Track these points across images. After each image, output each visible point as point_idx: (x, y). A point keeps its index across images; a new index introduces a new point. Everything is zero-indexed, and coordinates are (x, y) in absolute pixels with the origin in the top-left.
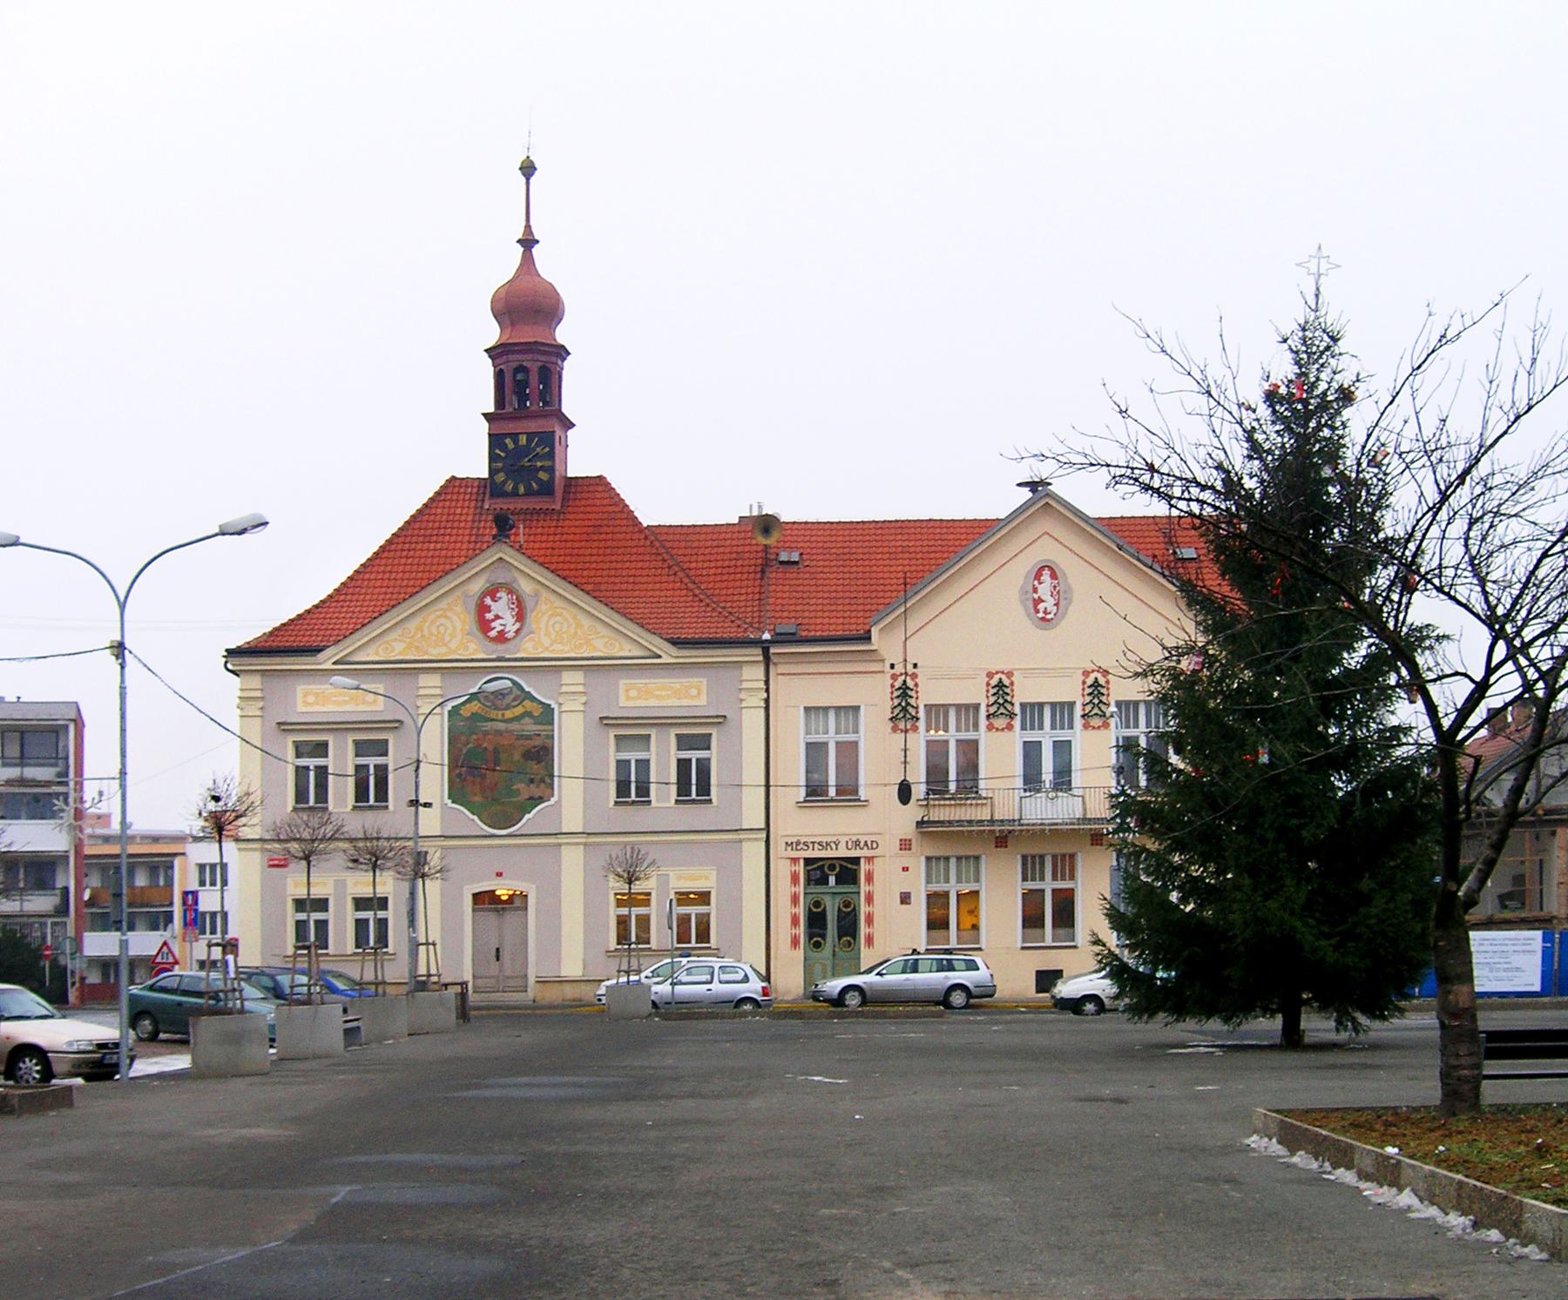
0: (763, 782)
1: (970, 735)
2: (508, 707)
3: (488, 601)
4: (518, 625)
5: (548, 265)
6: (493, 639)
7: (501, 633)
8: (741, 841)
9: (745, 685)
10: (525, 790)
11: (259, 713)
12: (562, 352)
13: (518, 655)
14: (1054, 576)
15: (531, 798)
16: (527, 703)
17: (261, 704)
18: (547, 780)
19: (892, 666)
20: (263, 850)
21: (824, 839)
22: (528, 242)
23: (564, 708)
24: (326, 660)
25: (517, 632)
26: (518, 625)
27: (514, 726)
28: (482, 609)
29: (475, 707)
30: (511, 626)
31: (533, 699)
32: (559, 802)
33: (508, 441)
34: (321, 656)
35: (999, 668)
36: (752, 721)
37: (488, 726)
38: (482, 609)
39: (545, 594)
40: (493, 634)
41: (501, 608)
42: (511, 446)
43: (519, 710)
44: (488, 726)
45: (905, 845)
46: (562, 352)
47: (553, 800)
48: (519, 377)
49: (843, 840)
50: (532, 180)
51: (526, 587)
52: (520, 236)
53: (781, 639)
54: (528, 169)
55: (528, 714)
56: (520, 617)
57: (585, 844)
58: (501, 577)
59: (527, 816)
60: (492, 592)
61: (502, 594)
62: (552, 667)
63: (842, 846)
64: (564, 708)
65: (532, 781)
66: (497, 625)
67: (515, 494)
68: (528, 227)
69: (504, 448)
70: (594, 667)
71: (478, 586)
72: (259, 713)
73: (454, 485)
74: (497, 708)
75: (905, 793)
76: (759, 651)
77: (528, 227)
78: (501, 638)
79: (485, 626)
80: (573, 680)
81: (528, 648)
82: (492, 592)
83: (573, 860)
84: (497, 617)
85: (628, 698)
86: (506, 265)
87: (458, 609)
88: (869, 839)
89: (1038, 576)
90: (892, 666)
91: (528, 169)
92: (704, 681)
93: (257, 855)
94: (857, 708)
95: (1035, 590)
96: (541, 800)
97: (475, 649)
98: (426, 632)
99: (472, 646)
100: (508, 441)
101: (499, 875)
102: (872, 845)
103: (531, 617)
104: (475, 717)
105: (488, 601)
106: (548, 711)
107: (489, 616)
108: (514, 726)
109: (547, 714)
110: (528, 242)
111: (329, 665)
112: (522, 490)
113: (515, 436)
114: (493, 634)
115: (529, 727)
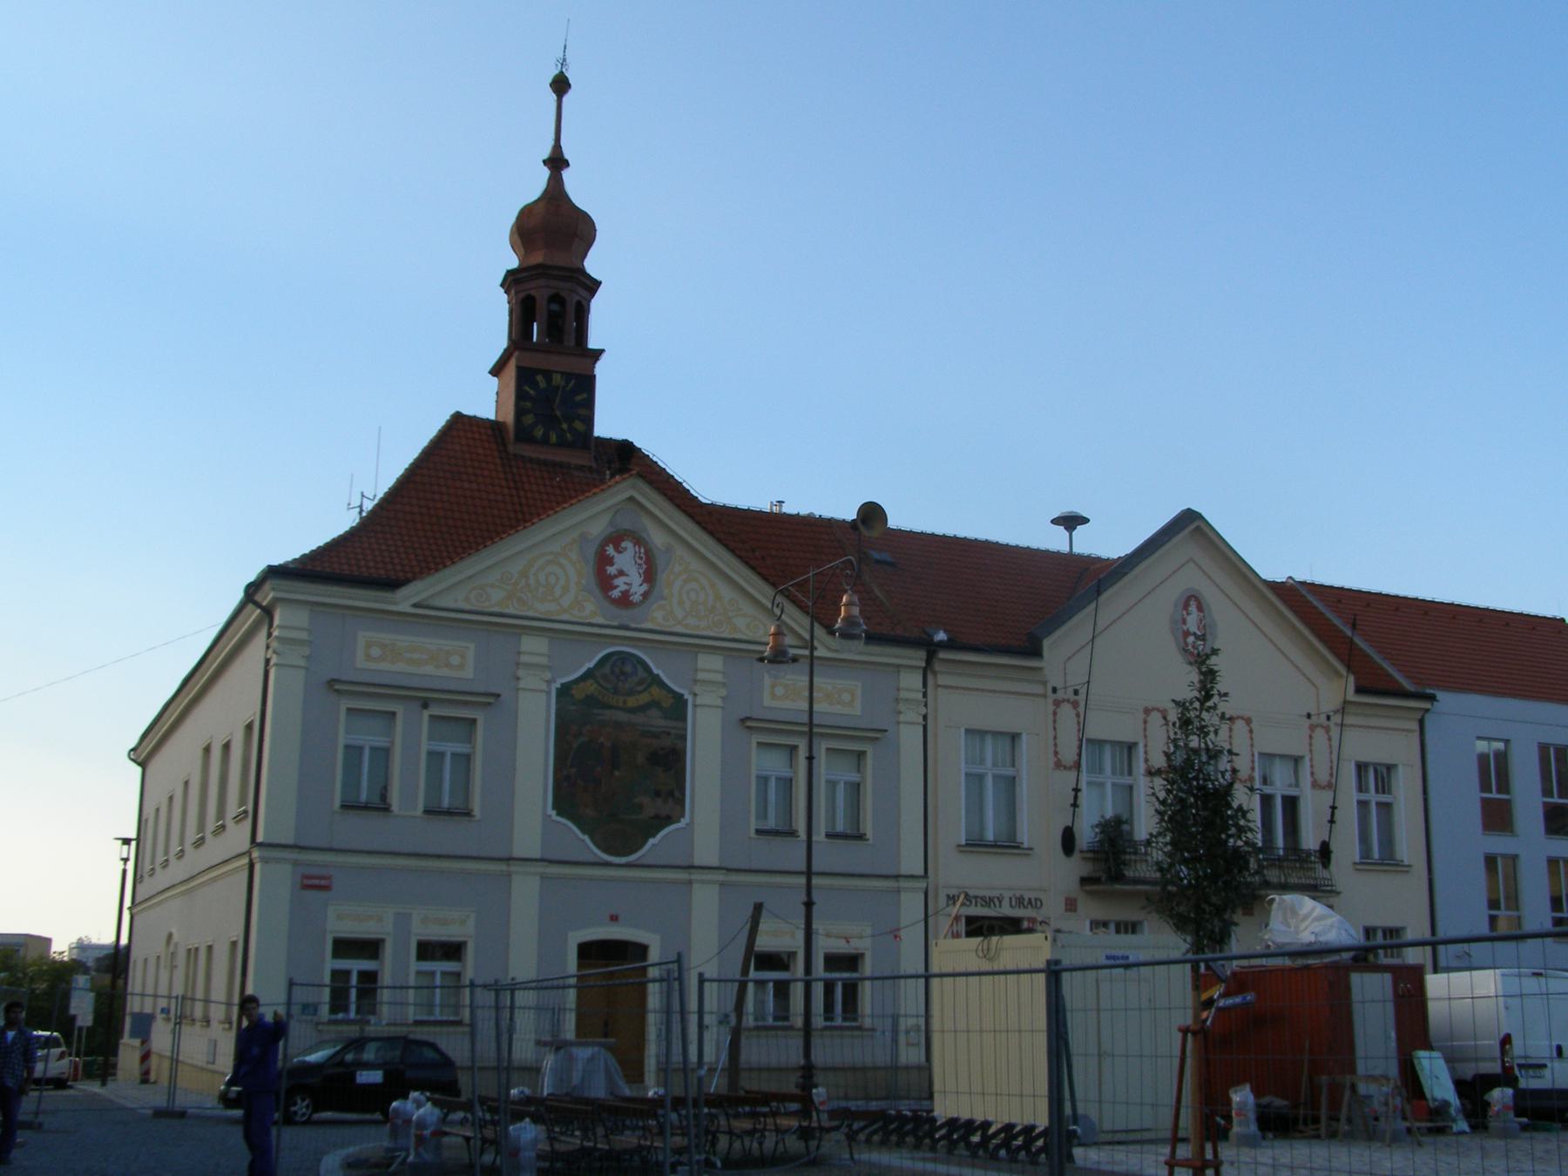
0: (1488, 944)
1: (1127, 780)
2: (631, 693)
3: (610, 550)
4: (645, 587)
5: (577, 188)
6: (615, 602)
7: (626, 594)
8: (898, 891)
9: (700, 676)
10: (651, 807)
11: (302, 663)
12: (593, 286)
13: (644, 626)
14: (1200, 608)
15: (657, 817)
16: (655, 690)
17: (307, 651)
18: (677, 794)
19: (1055, 690)
20: (296, 863)
21: (987, 893)
22: (557, 162)
23: (699, 701)
24: (404, 599)
25: (645, 595)
26: (645, 587)
27: (638, 719)
28: (603, 560)
29: (591, 687)
30: (638, 589)
31: (662, 685)
32: (690, 825)
33: (539, 378)
34: (402, 592)
35: (1240, 713)
36: (910, 738)
37: (609, 715)
38: (603, 560)
39: (680, 551)
40: (616, 593)
41: (626, 560)
42: (542, 383)
43: (644, 698)
44: (609, 715)
45: (1071, 905)
46: (593, 286)
47: (683, 822)
48: (555, 307)
49: (1007, 895)
50: (565, 99)
51: (658, 538)
52: (546, 156)
53: (950, 645)
54: (561, 85)
55: (654, 704)
56: (650, 576)
57: (722, 884)
58: (625, 523)
59: (651, 841)
60: (616, 539)
61: (627, 544)
62: (690, 646)
63: (1006, 903)
64: (699, 701)
65: (658, 794)
66: (620, 582)
67: (545, 441)
68: (557, 146)
69: (534, 385)
70: (732, 649)
71: (598, 529)
72: (302, 663)
73: (459, 423)
74: (616, 691)
75: (1068, 841)
76: (922, 654)
77: (557, 146)
78: (625, 601)
79: (605, 582)
80: (710, 664)
81: (656, 617)
82: (616, 539)
83: (705, 901)
84: (621, 573)
85: (369, 645)
86: (534, 184)
87: (574, 556)
88: (1033, 895)
89: (1186, 606)
90: (1055, 690)
91: (561, 85)
92: (472, 646)
93: (289, 867)
94: (1014, 737)
95: (1184, 622)
96: (668, 820)
97: (592, 610)
98: (532, 581)
99: (590, 607)
100: (539, 378)
101: (614, 918)
102: (1035, 903)
103: (662, 578)
104: (590, 701)
105: (610, 550)
106: (680, 702)
107: (611, 570)
108: (638, 719)
109: (677, 708)
110: (557, 162)
111: (405, 607)
112: (553, 438)
113: (547, 374)
114: (616, 593)
115: (656, 720)
